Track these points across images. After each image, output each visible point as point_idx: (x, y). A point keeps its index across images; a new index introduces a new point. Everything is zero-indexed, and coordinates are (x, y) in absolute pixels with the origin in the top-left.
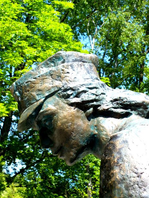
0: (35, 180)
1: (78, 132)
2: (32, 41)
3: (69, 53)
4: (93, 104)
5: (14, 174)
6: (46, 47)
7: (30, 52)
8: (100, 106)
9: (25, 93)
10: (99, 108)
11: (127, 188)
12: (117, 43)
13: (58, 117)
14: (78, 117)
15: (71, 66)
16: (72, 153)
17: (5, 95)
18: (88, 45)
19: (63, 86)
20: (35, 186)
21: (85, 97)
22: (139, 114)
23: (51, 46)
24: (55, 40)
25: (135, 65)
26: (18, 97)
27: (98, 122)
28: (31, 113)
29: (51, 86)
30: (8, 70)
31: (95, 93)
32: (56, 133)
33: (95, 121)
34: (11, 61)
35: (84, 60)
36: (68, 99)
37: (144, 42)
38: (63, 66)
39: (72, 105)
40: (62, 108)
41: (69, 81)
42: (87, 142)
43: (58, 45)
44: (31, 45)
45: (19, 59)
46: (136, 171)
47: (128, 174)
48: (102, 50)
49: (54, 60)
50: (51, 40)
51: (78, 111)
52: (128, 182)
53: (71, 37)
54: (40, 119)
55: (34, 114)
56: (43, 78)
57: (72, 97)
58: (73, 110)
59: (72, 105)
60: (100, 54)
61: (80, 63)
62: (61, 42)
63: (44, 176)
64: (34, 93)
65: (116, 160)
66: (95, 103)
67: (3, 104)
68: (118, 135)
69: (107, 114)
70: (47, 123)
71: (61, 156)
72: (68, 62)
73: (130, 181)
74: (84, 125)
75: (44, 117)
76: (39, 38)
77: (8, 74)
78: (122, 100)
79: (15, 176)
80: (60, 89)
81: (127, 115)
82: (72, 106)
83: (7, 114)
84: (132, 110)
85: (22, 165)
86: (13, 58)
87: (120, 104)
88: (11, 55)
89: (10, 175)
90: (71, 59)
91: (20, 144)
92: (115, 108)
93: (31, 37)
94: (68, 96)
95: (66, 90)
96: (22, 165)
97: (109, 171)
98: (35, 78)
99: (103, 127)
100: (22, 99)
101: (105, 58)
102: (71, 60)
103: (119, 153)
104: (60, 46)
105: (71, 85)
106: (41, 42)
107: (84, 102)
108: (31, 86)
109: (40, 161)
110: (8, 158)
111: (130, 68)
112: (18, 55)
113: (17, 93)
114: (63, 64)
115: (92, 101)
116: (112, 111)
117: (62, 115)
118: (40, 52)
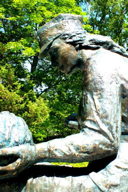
0: (54, 96)
1: (71, 58)
2: (49, 6)
3: (66, 14)
4: (79, 42)
5: (41, 92)
6: (58, 10)
7: (48, 14)
8: (83, 43)
9: (42, 37)
10: (82, 45)
11: (95, 84)
12: (105, 8)
13: (60, 50)
14: (71, 50)
15: (67, 22)
16: (68, 69)
17: (33, 42)
18: (87, 9)
19: (63, 33)
20: (54, 99)
21: (75, 39)
22: (104, 48)
23: (61, 10)
24: (65, 6)
25: (116, 23)
26: (39, 39)
27: (82, 52)
28: (46, 48)
29: (56, 33)
30: (34, 26)
31: (80, 36)
32: (59, 58)
33: (80, 52)
34: (35, 20)
35: (74, 18)
36: (66, 40)
37: (123, 6)
38: (63, 22)
39: (68, 43)
40: (62, 45)
41: (66, 30)
42: (76, 63)
43: (66, 9)
44: (49, 9)
45: (40, 19)
46: (99, 75)
47: (96, 77)
48: (95, 12)
49: (58, 18)
50: (62, 5)
51: (71, 46)
52: (95, 81)
53: (74, 4)
54: (51, 51)
55: (47, 48)
56: (52, 29)
57: (67, 39)
58: (68, 46)
59: (68, 43)
60: (94, 15)
61: (72, 20)
62: (68, 7)
63: (59, 93)
64: (47, 37)
65: (89, 70)
66: (80, 42)
67: (32, 48)
68: (91, 58)
69: (87, 48)
70: (55, 53)
71: (63, 71)
72: (65, 19)
73: (96, 81)
74: (74, 53)
75: (53, 50)
76: (53, 4)
77: (35, 29)
78: (95, 40)
79: (41, 94)
80: (61, 35)
81: (98, 48)
82: (68, 44)
83: (35, 54)
84: (100, 46)
85: (46, 86)
86: (37, 18)
87: (94, 42)
88: (35, 16)
89: (38, 93)
90: (67, 18)
91: (44, 74)
92: (91, 44)
93: (48, 4)
94: (66, 38)
95: (64, 35)
96: (46, 86)
97: (86, 76)
98: (48, 29)
99: (85, 55)
100: (41, 40)
101: (97, 18)
102: (67, 19)
103: (91, 67)
104: (67, 10)
105: (67, 32)
106: (55, 7)
107: (74, 42)
108: (45, 33)
109: (57, 83)
110: (36, 83)
111: (113, 24)
112: (40, 16)
113: (38, 37)
114: (63, 21)
115: (79, 41)
116: (90, 46)
117: (62, 48)
118: (54, 14)
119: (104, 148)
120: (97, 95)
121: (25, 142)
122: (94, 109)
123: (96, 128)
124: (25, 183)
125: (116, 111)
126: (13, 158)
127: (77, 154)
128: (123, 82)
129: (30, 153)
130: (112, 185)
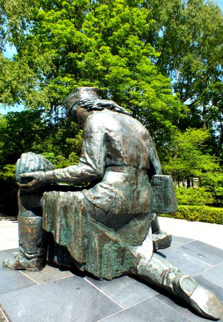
21: (86, 104)
51: (145, 137)
56: (72, 98)
58: (82, 109)
81: (103, 109)
90: (82, 90)
94: (80, 104)
119: (89, 174)
120: (88, 140)
121: (38, 170)
122: (85, 149)
123: (84, 161)
124: (42, 195)
125: (99, 150)
126: (30, 179)
127: (70, 177)
128: (107, 132)
129: (41, 176)
130: (95, 197)
